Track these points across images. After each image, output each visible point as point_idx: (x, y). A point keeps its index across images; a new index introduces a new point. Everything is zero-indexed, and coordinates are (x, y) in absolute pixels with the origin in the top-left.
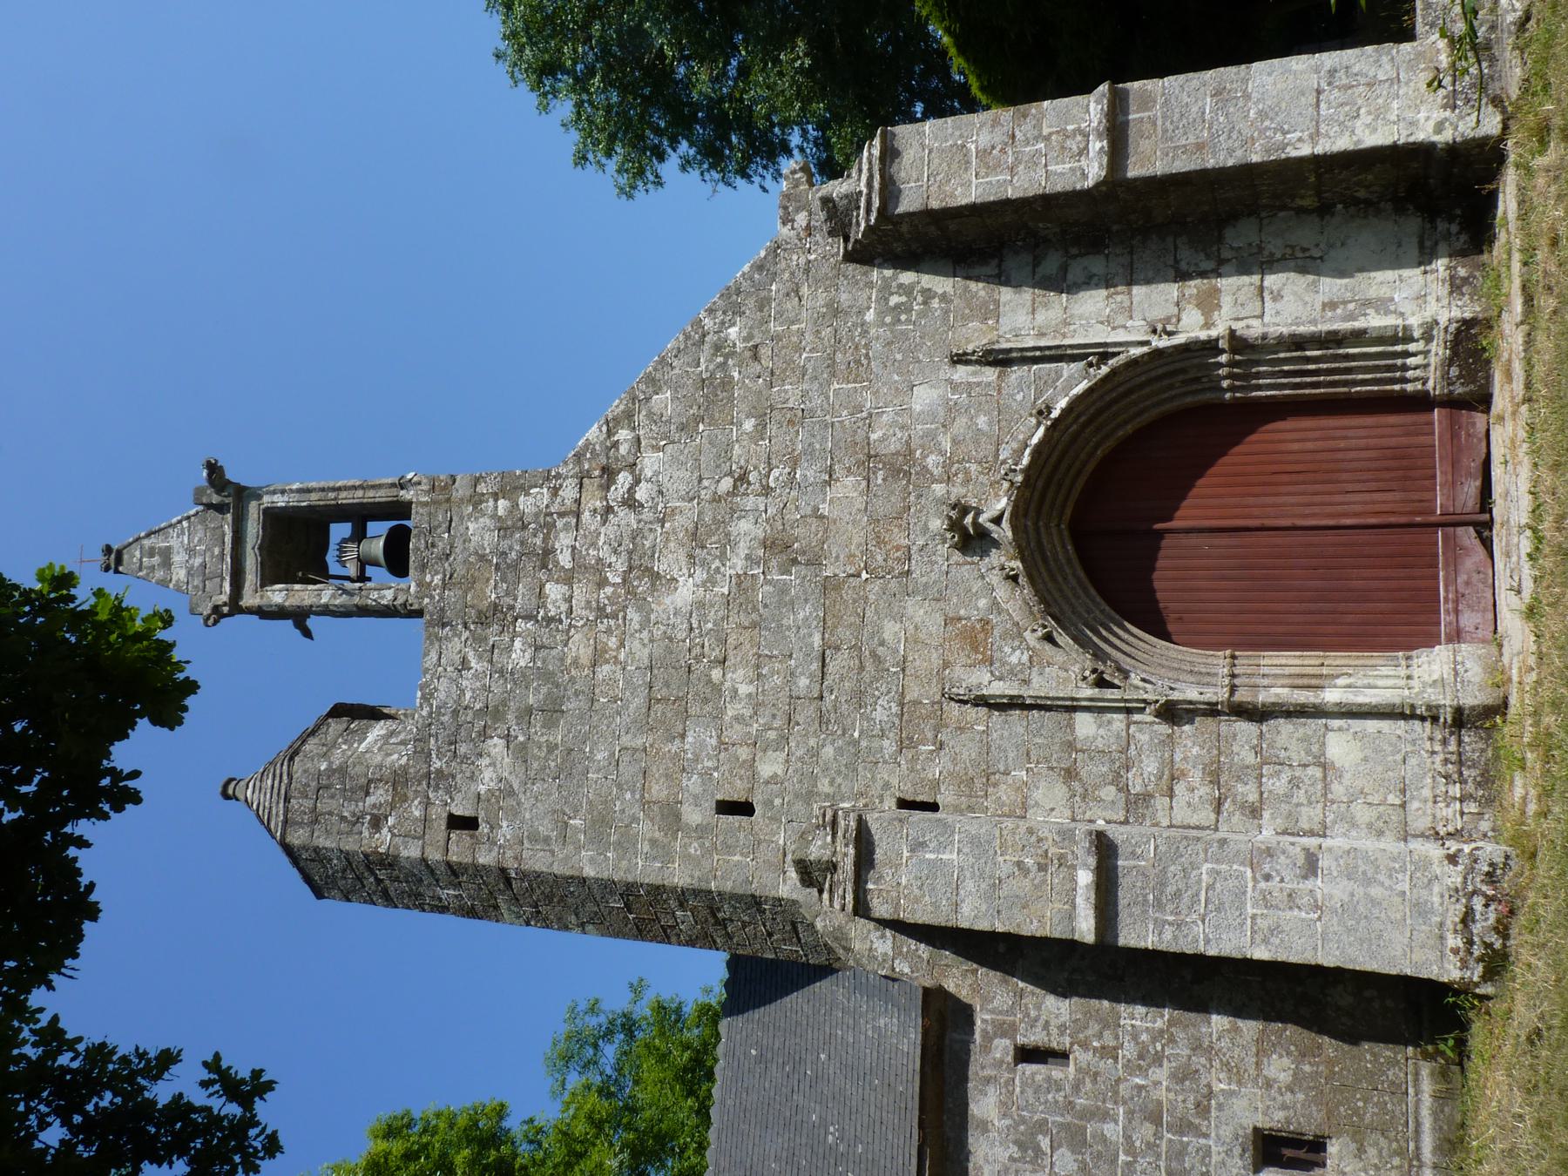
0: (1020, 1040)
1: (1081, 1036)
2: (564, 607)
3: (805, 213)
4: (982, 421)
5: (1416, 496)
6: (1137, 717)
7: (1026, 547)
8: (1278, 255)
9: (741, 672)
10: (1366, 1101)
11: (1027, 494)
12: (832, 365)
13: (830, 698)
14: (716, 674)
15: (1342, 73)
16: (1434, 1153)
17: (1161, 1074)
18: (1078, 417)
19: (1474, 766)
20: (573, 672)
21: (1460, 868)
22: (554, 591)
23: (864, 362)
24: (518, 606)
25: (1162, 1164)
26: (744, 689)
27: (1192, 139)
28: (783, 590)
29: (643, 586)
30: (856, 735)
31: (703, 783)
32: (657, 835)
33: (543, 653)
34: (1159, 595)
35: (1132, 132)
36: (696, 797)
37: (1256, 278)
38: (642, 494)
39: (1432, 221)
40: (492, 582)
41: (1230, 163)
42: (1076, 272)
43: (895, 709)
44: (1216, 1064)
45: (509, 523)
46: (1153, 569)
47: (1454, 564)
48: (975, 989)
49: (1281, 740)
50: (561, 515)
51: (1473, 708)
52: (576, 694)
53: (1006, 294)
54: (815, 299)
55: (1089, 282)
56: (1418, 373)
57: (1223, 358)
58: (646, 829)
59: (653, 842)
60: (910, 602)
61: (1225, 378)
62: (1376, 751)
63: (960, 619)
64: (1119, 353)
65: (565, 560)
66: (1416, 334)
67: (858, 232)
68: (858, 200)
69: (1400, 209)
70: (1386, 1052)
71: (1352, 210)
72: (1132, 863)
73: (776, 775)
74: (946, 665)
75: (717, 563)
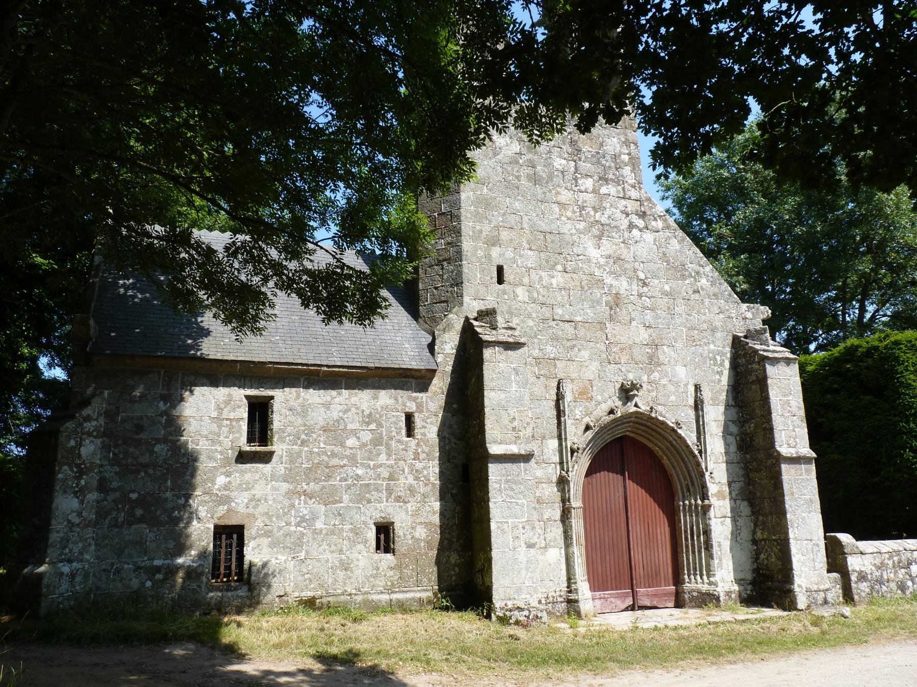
0: (416, 415)
1: (422, 443)
2: (583, 188)
3: (751, 317)
4: (673, 398)
5: (642, 580)
6: (558, 467)
7: (626, 418)
8: (737, 524)
9: (562, 280)
10: (413, 570)
11: (645, 418)
12: (692, 328)
13: (553, 324)
14: (559, 267)
15: (817, 549)
16: (396, 599)
17: (411, 480)
18: (675, 440)
19: (553, 608)
20: (553, 192)
21: (538, 605)
22: (589, 183)
23: (694, 344)
24: (581, 163)
25: (372, 481)
26: (554, 281)
27: (795, 490)
28: (598, 302)
29: (595, 231)
30: (539, 337)
31: (510, 259)
32: (484, 233)
33: (560, 175)
34: (598, 474)
35: (797, 466)
36: (504, 254)
37: (729, 515)
38: (635, 232)
39: (750, 583)
40: (591, 150)
41: (787, 506)
42: (731, 439)
43: (552, 356)
44: (419, 505)
45: (618, 161)
46: (608, 471)
47: (618, 597)
48: (435, 393)
49: (554, 529)
50: (623, 189)
51: (578, 607)
52: (544, 193)
53: (722, 408)
54: (718, 320)
55: (727, 445)
56: (693, 580)
57: (699, 502)
58: (486, 228)
59: (481, 231)
60: (597, 363)
61: (690, 503)
62: (553, 569)
63: (592, 387)
64: (701, 456)
65: (604, 190)
66: (711, 579)
67: (751, 343)
68: (765, 345)
69: (754, 571)
70: (434, 577)
71: (754, 552)
72: (523, 469)
73: (518, 296)
74: (572, 380)
75: (608, 270)
